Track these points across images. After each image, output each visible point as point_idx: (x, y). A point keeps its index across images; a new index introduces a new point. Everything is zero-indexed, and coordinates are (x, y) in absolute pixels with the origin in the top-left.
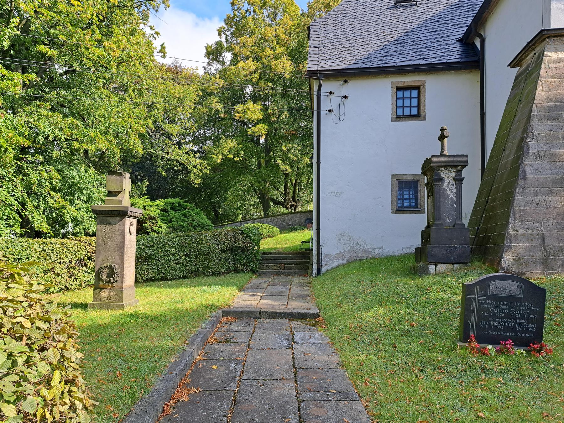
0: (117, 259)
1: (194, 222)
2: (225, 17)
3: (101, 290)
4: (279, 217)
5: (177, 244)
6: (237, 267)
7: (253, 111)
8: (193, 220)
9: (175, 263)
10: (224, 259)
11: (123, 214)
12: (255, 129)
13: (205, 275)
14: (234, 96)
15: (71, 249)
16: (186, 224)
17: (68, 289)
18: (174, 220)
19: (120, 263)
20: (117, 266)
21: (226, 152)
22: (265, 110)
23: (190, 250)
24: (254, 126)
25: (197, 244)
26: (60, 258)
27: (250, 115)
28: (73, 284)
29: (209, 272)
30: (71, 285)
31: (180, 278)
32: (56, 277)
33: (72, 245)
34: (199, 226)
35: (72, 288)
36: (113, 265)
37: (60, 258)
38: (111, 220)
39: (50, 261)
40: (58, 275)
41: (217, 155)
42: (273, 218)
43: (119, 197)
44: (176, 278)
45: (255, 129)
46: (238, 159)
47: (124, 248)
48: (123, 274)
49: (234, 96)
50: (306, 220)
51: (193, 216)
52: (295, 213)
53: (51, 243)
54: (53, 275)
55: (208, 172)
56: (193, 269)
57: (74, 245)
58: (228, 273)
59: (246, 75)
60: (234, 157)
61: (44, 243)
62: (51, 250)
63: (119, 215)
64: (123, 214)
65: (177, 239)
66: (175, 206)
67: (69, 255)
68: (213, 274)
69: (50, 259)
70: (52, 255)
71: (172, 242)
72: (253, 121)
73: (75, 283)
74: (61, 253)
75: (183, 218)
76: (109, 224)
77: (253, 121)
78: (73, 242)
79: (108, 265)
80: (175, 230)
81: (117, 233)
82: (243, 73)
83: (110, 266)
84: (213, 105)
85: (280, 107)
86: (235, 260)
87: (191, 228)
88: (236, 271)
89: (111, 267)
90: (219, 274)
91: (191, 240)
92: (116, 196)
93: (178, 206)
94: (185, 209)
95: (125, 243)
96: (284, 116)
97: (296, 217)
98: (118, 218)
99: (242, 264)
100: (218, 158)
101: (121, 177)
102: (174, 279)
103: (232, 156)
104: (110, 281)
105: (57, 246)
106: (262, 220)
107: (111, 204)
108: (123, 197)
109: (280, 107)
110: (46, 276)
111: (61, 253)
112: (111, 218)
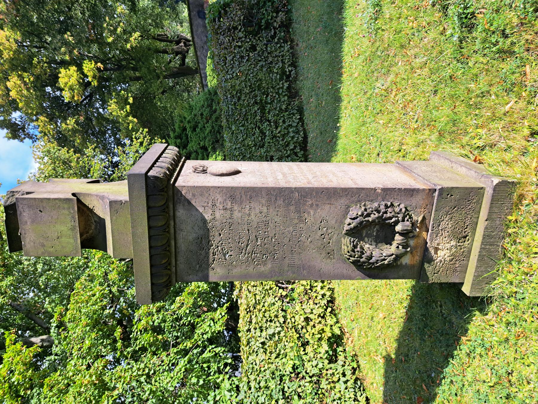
0: (327, 212)
1: (205, 114)
2: (6, 139)
3: (430, 260)
4: (199, 53)
5: (243, 126)
6: (282, 22)
7: (68, 77)
8: (202, 114)
9: (277, 128)
10: (267, 45)
11: (160, 196)
12: (90, 74)
13: (296, 79)
14: (58, 109)
15: (258, 297)
16: (208, 125)
17: (332, 301)
18: (202, 143)
19: (343, 201)
20: (355, 211)
21: (123, 113)
22: (64, 64)
23: (253, 105)
24: (87, 76)
25: (240, 93)
26: (276, 316)
27: (73, 81)
28: (322, 292)
29: (290, 72)
30: (323, 295)
31: (301, 120)
32: (311, 323)
33: (250, 295)
34: (210, 106)
35: (328, 294)
36: (348, 224)
37: (276, 316)
38: (186, 235)
39: (282, 334)
40: (307, 319)
41: (129, 124)
42: (200, 61)
43: (102, 211)
44: (303, 125)
45: (90, 74)
46: (131, 99)
47: (290, 191)
48: (385, 190)
49: (58, 109)
50: (200, 17)
51: (195, 115)
52: (193, 41)
53: (249, 330)
54: (309, 328)
55: (146, 130)
56: (286, 98)
57: (250, 292)
58: (292, 41)
59: (28, 89)
60: (129, 104)
61: (248, 343)
62: (262, 331)
63: (165, 209)
64: (160, 196)
65: (234, 128)
66: (181, 143)
67: (270, 300)
68: (294, 65)
69: (279, 333)
70: (270, 331)
71: (240, 137)
72: (80, 78)
73: (319, 289)
74: (267, 315)
75: (198, 130)
76: (203, 240)
77: (80, 78)
78: (245, 293)
79: (346, 243)
80: (217, 141)
81: (237, 215)
82: (25, 92)
83: (351, 233)
84: (70, 127)
85: (59, 44)
86: (268, 26)
87: (214, 117)
88: (287, 25)
89: (356, 233)
90: (294, 55)
91: (235, 104)
92: (101, 222)
93: (181, 139)
94: (185, 129)
95: (271, 185)
96: (71, 38)
97: (197, 31)
98: (181, 213)
99: (275, 15)
100: (132, 122)
101: (20, 208)
102: (304, 130)
103: (128, 107)
104: (405, 234)
105: (254, 321)
106: (203, 75)
107: (128, 238)
108: (102, 198)
109: (59, 44)
110: (311, 342)
111: (267, 315)
112: (181, 236)
